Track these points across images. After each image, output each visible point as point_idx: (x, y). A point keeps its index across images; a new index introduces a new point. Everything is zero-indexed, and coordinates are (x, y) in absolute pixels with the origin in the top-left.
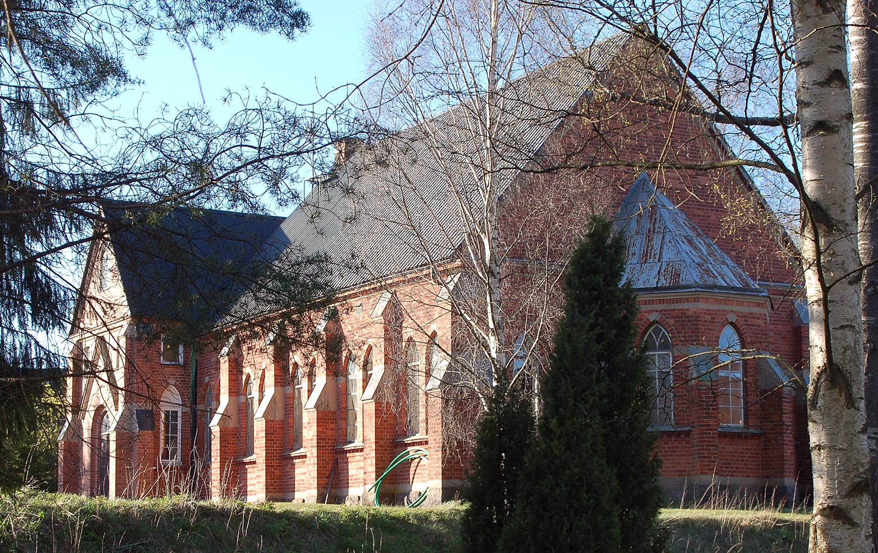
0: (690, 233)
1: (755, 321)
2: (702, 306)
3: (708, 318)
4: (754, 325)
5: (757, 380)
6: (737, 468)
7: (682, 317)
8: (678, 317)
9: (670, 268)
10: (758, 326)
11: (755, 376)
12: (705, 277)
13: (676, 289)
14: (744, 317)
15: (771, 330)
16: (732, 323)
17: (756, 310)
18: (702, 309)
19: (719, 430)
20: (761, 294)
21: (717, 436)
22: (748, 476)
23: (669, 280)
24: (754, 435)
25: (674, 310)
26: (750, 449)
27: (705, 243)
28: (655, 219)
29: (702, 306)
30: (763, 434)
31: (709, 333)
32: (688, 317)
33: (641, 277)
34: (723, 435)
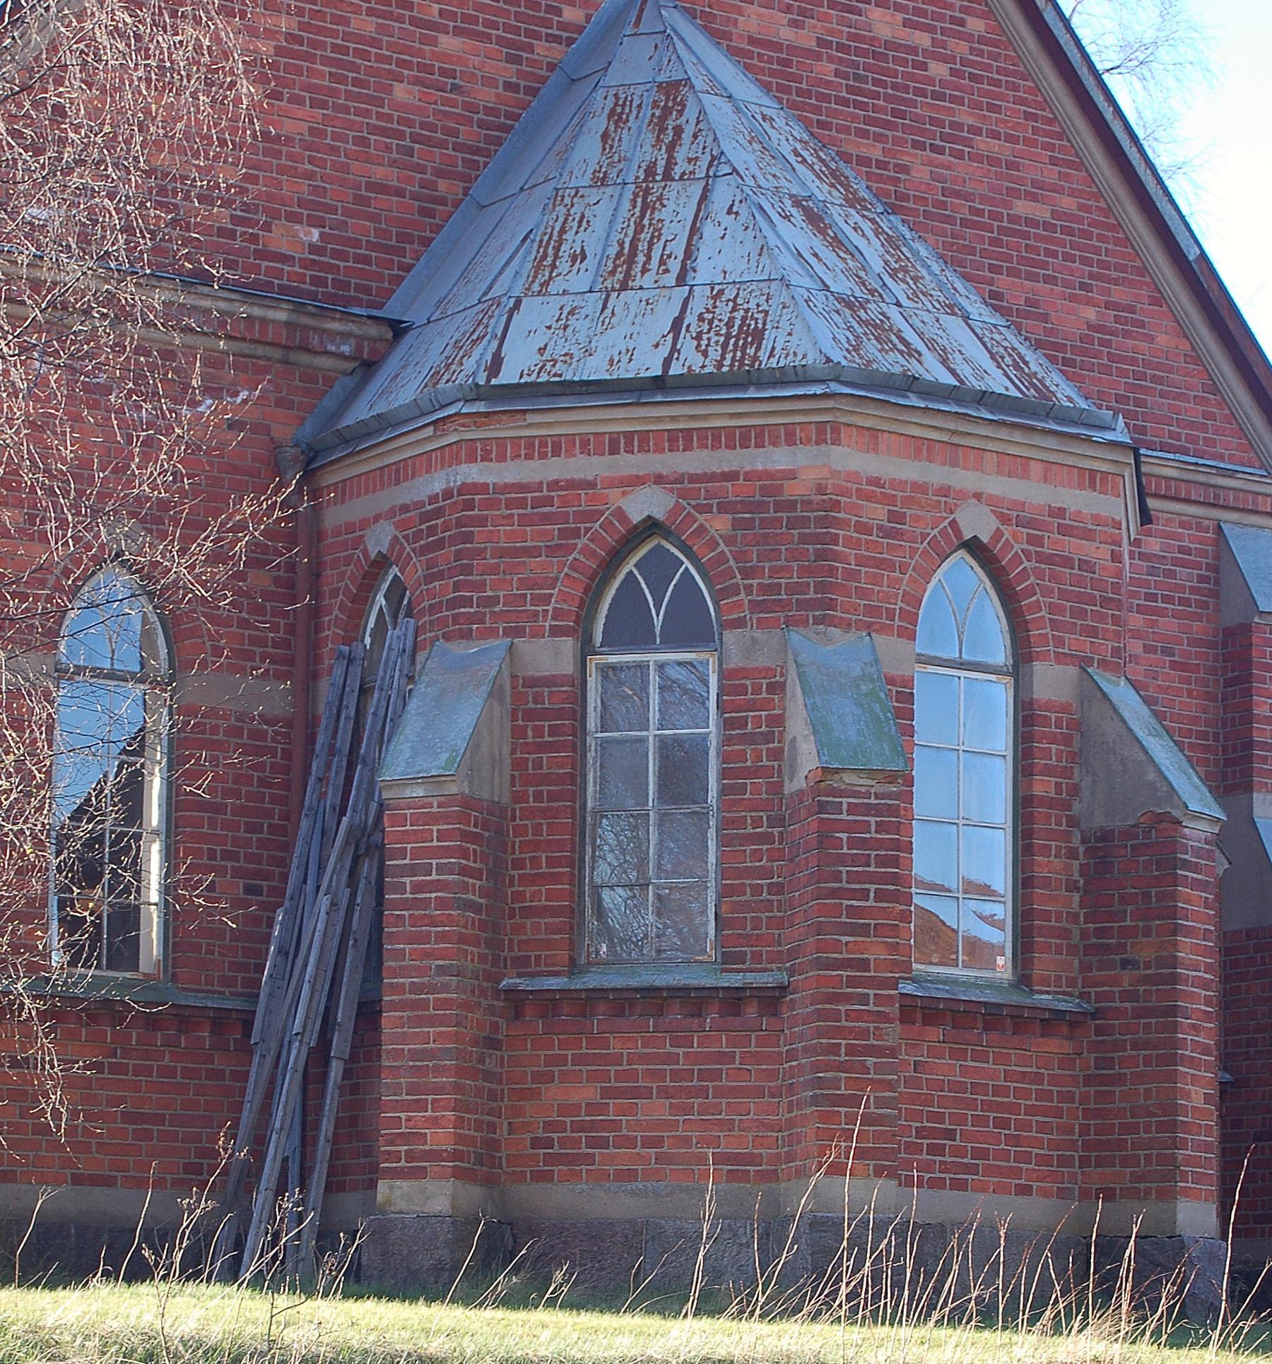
0: (820, 190)
1: (1073, 547)
2: (849, 459)
3: (877, 513)
4: (1067, 562)
5: (1075, 790)
6: (980, 1154)
7: (761, 506)
8: (748, 506)
9: (723, 310)
10: (1086, 565)
11: (1066, 772)
12: (871, 347)
13: (744, 386)
14: (1029, 524)
15: (1136, 635)
16: (975, 547)
17: (1079, 501)
18: (853, 476)
19: (907, 988)
20: (1098, 436)
21: (894, 1011)
22: (1025, 1190)
23: (715, 354)
24: (1050, 1022)
25: (731, 476)
26: (1038, 1078)
27: (878, 232)
28: (678, 131)
29: (849, 459)
30: (1094, 1016)
31: (876, 580)
32: (791, 505)
33: (601, 343)
34: (924, 1012)
